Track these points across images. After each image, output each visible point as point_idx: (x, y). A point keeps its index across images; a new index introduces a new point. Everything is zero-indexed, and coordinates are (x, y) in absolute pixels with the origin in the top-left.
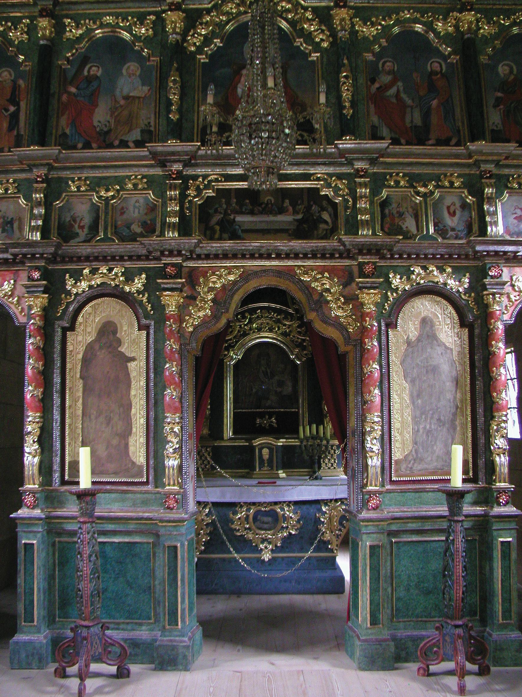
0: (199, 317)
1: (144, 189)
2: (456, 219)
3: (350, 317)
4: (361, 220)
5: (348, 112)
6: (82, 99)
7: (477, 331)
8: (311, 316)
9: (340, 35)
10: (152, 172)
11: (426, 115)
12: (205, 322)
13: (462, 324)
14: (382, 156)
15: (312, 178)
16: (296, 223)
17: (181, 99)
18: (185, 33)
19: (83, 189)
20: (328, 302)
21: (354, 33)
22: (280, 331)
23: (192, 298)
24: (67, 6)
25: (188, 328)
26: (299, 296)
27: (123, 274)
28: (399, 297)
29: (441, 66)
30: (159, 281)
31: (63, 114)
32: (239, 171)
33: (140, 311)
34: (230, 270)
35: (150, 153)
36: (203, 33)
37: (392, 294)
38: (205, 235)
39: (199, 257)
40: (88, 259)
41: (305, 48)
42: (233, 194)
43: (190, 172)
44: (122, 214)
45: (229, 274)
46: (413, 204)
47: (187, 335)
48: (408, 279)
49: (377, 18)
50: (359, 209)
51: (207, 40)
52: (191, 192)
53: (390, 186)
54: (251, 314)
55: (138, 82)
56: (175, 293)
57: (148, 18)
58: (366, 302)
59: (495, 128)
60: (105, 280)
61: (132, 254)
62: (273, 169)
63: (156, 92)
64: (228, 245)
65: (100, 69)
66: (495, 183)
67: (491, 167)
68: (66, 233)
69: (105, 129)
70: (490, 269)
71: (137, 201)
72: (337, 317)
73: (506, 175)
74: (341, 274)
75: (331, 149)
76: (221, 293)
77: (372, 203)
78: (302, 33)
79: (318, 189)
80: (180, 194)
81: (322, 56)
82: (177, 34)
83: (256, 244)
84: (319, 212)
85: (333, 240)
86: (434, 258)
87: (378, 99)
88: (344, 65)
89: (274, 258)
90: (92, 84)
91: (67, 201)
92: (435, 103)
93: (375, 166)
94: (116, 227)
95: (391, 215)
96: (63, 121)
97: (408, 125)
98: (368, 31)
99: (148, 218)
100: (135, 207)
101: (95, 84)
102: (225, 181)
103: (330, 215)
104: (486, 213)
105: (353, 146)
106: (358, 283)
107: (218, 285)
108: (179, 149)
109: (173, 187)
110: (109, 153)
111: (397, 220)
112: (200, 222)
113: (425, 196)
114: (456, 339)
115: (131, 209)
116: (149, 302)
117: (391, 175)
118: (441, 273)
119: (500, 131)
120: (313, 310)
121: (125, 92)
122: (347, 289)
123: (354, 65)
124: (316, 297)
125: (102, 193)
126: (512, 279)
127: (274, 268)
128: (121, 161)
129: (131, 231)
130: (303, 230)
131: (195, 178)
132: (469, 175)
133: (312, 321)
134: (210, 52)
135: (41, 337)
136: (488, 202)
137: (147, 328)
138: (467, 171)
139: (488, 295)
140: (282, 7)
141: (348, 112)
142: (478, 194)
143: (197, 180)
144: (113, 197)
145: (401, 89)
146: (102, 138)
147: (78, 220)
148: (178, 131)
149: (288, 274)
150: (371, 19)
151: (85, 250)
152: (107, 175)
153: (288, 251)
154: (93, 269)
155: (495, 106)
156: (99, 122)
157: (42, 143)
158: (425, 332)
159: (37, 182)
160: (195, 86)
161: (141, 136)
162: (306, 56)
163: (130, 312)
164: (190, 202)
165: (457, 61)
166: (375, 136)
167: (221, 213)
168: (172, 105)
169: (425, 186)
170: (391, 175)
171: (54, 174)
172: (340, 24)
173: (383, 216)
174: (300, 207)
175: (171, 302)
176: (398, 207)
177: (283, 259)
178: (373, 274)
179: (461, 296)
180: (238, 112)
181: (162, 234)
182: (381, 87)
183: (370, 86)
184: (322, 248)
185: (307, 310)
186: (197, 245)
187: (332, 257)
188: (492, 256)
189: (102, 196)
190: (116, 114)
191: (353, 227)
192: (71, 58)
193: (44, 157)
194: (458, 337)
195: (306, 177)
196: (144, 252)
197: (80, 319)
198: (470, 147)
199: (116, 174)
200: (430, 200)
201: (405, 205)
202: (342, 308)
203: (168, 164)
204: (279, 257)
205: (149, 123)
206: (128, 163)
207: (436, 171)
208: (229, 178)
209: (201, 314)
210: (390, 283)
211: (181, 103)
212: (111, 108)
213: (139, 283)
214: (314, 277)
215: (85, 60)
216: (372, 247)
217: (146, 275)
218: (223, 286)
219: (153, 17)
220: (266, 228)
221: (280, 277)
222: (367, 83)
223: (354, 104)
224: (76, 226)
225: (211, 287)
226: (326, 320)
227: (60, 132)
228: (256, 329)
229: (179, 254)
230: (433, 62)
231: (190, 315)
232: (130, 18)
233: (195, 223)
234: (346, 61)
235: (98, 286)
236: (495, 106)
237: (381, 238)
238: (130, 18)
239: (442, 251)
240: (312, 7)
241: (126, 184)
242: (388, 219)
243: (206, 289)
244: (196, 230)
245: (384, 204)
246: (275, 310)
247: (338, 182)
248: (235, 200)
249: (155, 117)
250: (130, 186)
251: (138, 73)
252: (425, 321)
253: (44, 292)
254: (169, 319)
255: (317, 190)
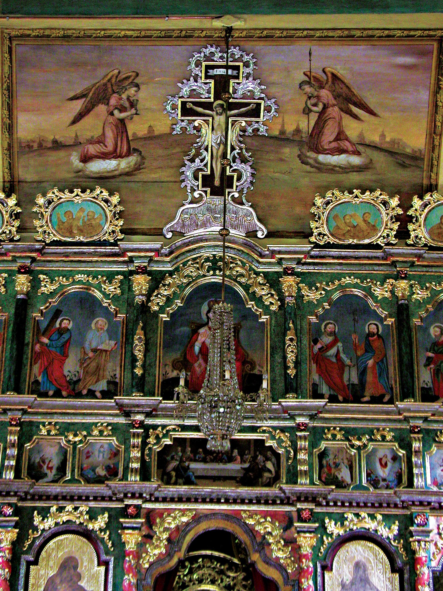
0: (155, 555)
1: (109, 436)
2: (387, 470)
3: (290, 558)
4: (301, 470)
5: (291, 372)
6: (54, 349)
7: (406, 576)
8: (255, 557)
9: (287, 300)
10: (116, 420)
11: (362, 374)
12: (160, 559)
13: (393, 570)
14: (321, 412)
15: (258, 431)
16: (242, 471)
17: (145, 356)
18: (149, 296)
19: (53, 432)
20: (269, 544)
21: (300, 297)
22: (224, 584)
23: (149, 537)
24: (42, 263)
25: (144, 564)
26: (244, 538)
27: (87, 513)
28: (334, 542)
29: (378, 328)
30: (121, 520)
31: (35, 363)
32: (193, 422)
33: (102, 547)
34: (184, 512)
35: (117, 404)
36: (166, 293)
37: (327, 539)
38: (162, 480)
39: (157, 500)
40: (56, 498)
41: (256, 310)
42: (188, 443)
43: (150, 421)
44: (88, 457)
45: (183, 515)
46: (348, 457)
47: (143, 571)
48: (342, 525)
49: (321, 283)
50: (299, 460)
51: (169, 300)
52: (151, 440)
53: (327, 439)
54: (192, 564)
55: (105, 336)
56: (136, 532)
57: (116, 277)
58: (303, 545)
59: (425, 386)
60: (71, 518)
61: (98, 495)
62: (227, 436)
63: (122, 346)
64: (183, 489)
65: (71, 322)
66: (423, 437)
67: (419, 423)
68: (36, 473)
69: (75, 379)
70: (416, 517)
71: (102, 447)
72: (278, 558)
73: (434, 430)
74: (282, 518)
75: (275, 406)
76: (175, 533)
77: (311, 455)
78: (253, 296)
79: (264, 440)
80: (142, 441)
81: (271, 319)
82: (142, 295)
83: (208, 490)
84: (264, 462)
85: (275, 487)
86: (366, 505)
87: (319, 359)
88: (289, 329)
89: (222, 503)
90: (63, 336)
91: (38, 443)
92: (371, 362)
93: (314, 420)
94: (82, 470)
95: (329, 466)
96: (36, 368)
97: (346, 383)
98: (312, 296)
99: (111, 463)
100: (100, 451)
101: (66, 336)
102: (181, 431)
103: (274, 465)
104: (414, 465)
105: (295, 403)
106: (296, 528)
107: (173, 526)
108: (143, 402)
109: (136, 435)
110: (79, 403)
111: (333, 471)
112: (158, 468)
113: (359, 448)
114: (388, 583)
115: (96, 453)
116: (110, 539)
117: (329, 429)
118: (372, 519)
119: (430, 388)
120: (256, 551)
121: (94, 345)
122: (288, 533)
123: (299, 327)
124: (259, 539)
125: (71, 437)
126: (438, 528)
127: (223, 512)
128: (89, 410)
129: (95, 473)
130: (250, 478)
131: (155, 427)
132: (400, 429)
133: (255, 562)
134: (171, 312)
135: (9, 569)
136: (415, 455)
137: (106, 564)
138: (399, 426)
139: (414, 541)
140: (237, 272)
141: (291, 372)
142: (406, 444)
143: (156, 429)
144: (81, 442)
145: (341, 349)
146: (71, 387)
147: (47, 462)
148: (141, 385)
149: (234, 517)
150: (315, 284)
151: (56, 489)
152: (76, 421)
153: (236, 497)
154: (60, 507)
155: (426, 366)
156: (69, 371)
157: (18, 390)
158: (359, 576)
159: (12, 425)
160: (157, 343)
161: (108, 386)
162: (257, 317)
163: (90, 548)
164: (150, 449)
165: (392, 323)
166: (316, 395)
167: (176, 460)
168: (136, 361)
169: (359, 439)
170: (329, 429)
171: (26, 418)
172: (288, 291)
173: (321, 466)
174: (247, 457)
175: (131, 539)
176: (335, 458)
177: (231, 503)
178: (310, 519)
179: (391, 543)
180: (202, 391)
181: (125, 478)
182: (323, 347)
183: (313, 347)
184: (265, 495)
185: (251, 552)
186: (156, 489)
187: (274, 503)
188: (417, 505)
189: (70, 441)
190: (85, 365)
191: (293, 478)
192: (44, 311)
193: (21, 403)
194: (389, 581)
195: (254, 429)
196: (109, 493)
197: (43, 553)
198: (399, 406)
199: (84, 421)
200: (364, 453)
201: (340, 457)
202: (283, 550)
203: (132, 415)
204: (227, 501)
205: (115, 375)
206: (96, 411)
207: (370, 425)
208: (184, 428)
209: (157, 552)
210: (326, 529)
211: (145, 359)
212: (80, 360)
213: (101, 522)
214: (258, 521)
215: (57, 313)
216: (308, 495)
217: (109, 514)
218: (177, 527)
219: (121, 277)
220: (217, 475)
221: (228, 520)
222: (310, 342)
223: (297, 364)
224: (45, 467)
225: (166, 528)
226: (268, 561)
227: (32, 380)
228: (196, 580)
229: (141, 496)
230: (371, 324)
231: (147, 552)
232: (100, 277)
233: (154, 469)
234: (291, 325)
235: (64, 523)
236: (426, 366)
237: (319, 488)
238: (100, 277)
239: (372, 499)
240: (263, 273)
241: (92, 431)
242: (326, 470)
243: (161, 529)
244: (154, 475)
245: (322, 455)
246: (218, 559)
247: (282, 435)
248: (190, 449)
249: (121, 370)
250: (96, 432)
251: (106, 328)
252: (357, 565)
253: (15, 527)
254: (129, 555)
255: (263, 441)
